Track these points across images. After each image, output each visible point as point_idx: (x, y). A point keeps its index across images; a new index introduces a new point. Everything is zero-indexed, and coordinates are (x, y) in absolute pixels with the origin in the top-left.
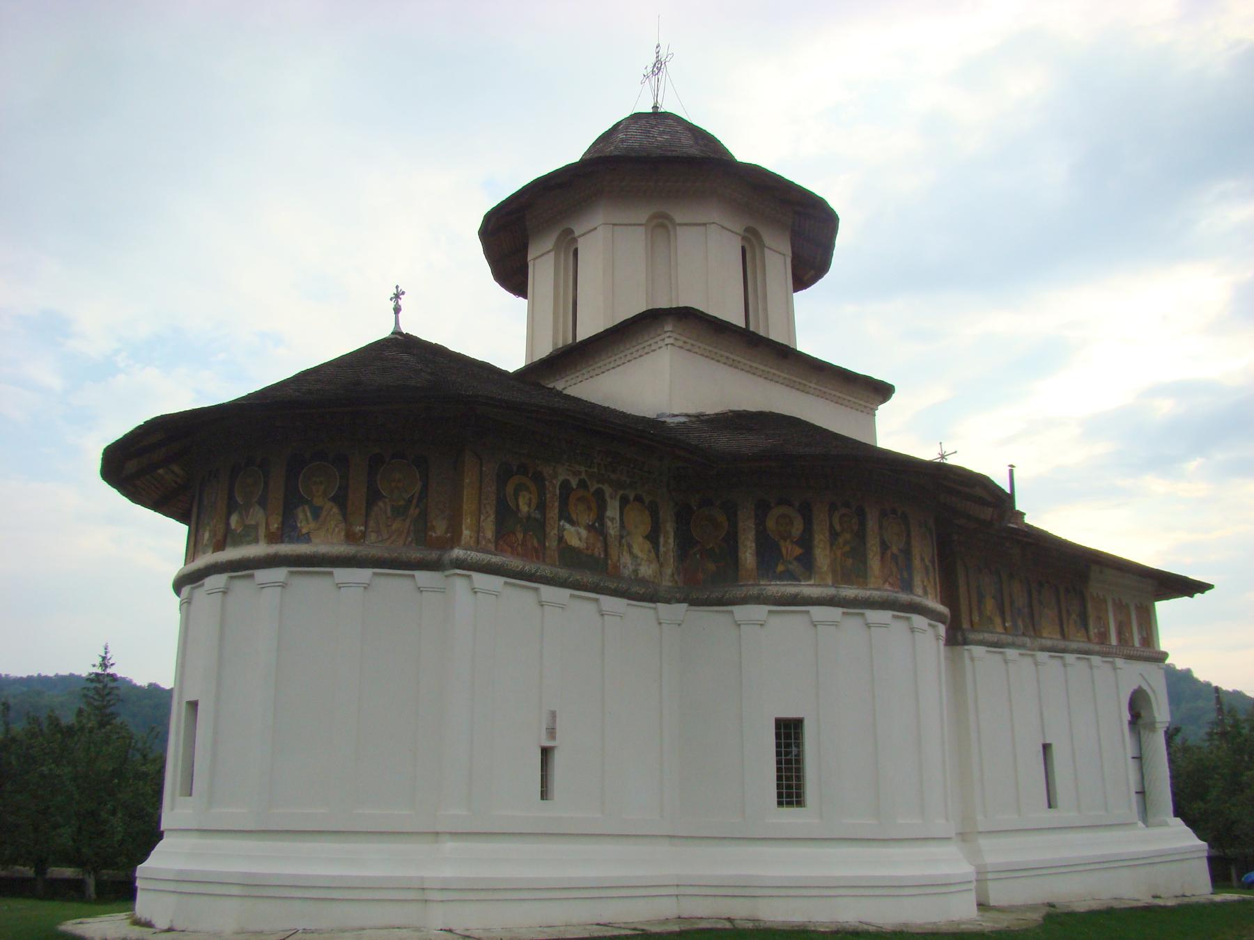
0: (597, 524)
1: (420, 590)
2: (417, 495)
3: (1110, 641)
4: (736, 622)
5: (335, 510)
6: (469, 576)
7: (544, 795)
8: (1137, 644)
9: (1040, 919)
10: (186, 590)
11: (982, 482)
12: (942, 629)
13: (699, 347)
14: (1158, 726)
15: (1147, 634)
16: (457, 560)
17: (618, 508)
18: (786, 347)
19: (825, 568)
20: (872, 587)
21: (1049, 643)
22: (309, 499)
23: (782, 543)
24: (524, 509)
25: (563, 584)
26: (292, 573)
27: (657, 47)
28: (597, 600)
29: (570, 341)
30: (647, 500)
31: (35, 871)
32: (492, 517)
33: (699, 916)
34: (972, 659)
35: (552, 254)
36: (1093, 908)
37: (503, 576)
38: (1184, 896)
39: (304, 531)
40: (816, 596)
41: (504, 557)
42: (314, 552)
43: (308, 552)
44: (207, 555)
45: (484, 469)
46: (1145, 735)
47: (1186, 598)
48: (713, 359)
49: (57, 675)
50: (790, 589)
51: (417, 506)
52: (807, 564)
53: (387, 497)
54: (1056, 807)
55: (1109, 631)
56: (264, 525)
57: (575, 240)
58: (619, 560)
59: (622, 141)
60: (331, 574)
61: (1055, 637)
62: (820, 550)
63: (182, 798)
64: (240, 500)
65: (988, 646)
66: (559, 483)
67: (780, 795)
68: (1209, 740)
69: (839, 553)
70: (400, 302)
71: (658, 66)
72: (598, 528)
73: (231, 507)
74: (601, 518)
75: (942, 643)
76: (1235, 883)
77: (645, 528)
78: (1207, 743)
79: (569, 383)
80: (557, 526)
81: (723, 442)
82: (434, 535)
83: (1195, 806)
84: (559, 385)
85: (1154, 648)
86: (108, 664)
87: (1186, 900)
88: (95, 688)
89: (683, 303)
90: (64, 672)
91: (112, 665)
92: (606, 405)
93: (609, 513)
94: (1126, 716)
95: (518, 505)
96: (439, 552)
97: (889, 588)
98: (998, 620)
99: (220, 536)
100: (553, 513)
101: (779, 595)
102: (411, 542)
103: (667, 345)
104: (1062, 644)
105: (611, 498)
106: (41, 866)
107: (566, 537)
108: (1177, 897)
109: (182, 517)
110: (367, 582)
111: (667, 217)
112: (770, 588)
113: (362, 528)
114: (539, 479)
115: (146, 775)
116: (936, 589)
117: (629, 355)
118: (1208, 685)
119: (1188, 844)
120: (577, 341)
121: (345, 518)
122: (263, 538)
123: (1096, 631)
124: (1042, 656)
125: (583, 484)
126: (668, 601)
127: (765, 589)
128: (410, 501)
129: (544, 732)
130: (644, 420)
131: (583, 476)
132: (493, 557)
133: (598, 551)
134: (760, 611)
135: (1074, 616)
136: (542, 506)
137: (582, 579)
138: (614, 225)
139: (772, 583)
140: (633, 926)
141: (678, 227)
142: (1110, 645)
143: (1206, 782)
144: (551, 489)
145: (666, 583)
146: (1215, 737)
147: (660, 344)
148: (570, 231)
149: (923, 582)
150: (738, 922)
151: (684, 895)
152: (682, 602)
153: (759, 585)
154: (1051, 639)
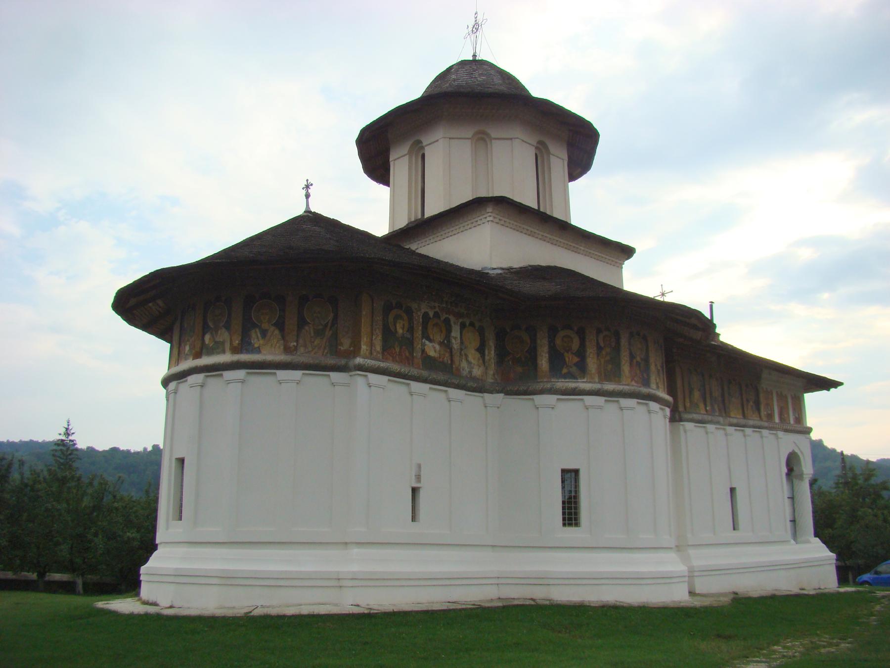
0: (446, 341)
1: (333, 384)
2: (330, 322)
3: (774, 420)
4: (535, 406)
5: (277, 332)
6: (366, 376)
7: (414, 519)
8: (792, 422)
9: (730, 601)
10: (172, 385)
11: (695, 315)
12: (668, 411)
13: (509, 223)
14: (805, 476)
15: (799, 415)
16: (359, 365)
17: (459, 330)
18: (566, 222)
19: (593, 371)
20: (624, 383)
21: (735, 421)
22: (259, 324)
23: (566, 354)
24: (400, 331)
25: (425, 381)
26: (248, 373)
27: (475, 14)
28: (446, 391)
29: (419, 216)
30: (477, 325)
31: (37, 575)
32: (380, 337)
33: (512, 597)
34: (685, 431)
35: (408, 156)
36: (762, 595)
37: (387, 375)
38: (820, 589)
39: (256, 346)
40: (588, 389)
41: (388, 363)
42: (264, 360)
43: (260, 360)
44: (188, 361)
45: (374, 305)
46: (796, 481)
47: (825, 392)
48: (518, 231)
49: (21, 441)
50: (571, 385)
51: (331, 329)
52: (582, 369)
53: (310, 324)
54: (738, 530)
55: (774, 413)
56: (229, 342)
57: (423, 148)
58: (460, 365)
59: (454, 80)
60: (275, 374)
61: (738, 417)
62: (590, 359)
63: (174, 521)
64: (211, 324)
65: (696, 423)
66: (422, 315)
67: (564, 519)
68: (836, 488)
69: (602, 361)
70: (309, 191)
71: (476, 27)
72: (446, 344)
73: (205, 329)
74: (448, 336)
75: (668, 420)
76: (851, 582)
77: (477, 344)
78: (834, 491)
79: (420, 245)
80: (420, 342)
81: (528, 287)
82: (342, 348)
83: (826, 532)
84: (413, 247)
85: (803, 424)
86: (70, 433)
87: (821, 591)
88: (61, 450)
89: (497, 193)
90: (26, 439)
91: (73, 433)
92: (446, 261)
93: (453, 334)
94: (785, 470)
95: (396, 329)
96: (346, 360)
97: (635, 384)
98: (702, 405)
99: (198, 349)
100: (418, 333)
101: (564, 388)
102: (327, 353)
103: (488, 221)
104: (743, 421)
105: (455, 323)
106: (41, 575)
107: (426, 350)
108: (815, 589)
109: (163, 334)
110: (242, 378)
111: (484, 133)
112: (558, 384)
113: (295, 344)
114: (409, 312)
115: (117, 509)
116: (664, 385)
117: (462, 228)
118: (834, 451)
119: (823, 555)
120: (426, 216)
121: (283, 338)
122: (228, 350)
123: (765, 413)
124: (731, 429)
125: (436, 315)
126: (491, 392)
127: (554, 385)
128: (326, 326)
129: (414, 477)
130: (472, 272)
131: (437, 309)
132: (382, 363)
133: (447, 359)
134: (551, 399)
135: (751, 403)
136: (411, 329)
137: (437, 377)
138: (450, 138)
139: (560, 380)
140: (473, 603)
141: (493, 141)
142: (775, 422)
143: (834, 515)
144: (417, 318)
145: (490, 380)
146: (841, 486)
147: (484, 221)
148: (420, 142)
149: (656, 380)
150: (538, 600)
151: (502, 584)
152: (501, 393)
153: (551, 382)
154: (736, 418)
